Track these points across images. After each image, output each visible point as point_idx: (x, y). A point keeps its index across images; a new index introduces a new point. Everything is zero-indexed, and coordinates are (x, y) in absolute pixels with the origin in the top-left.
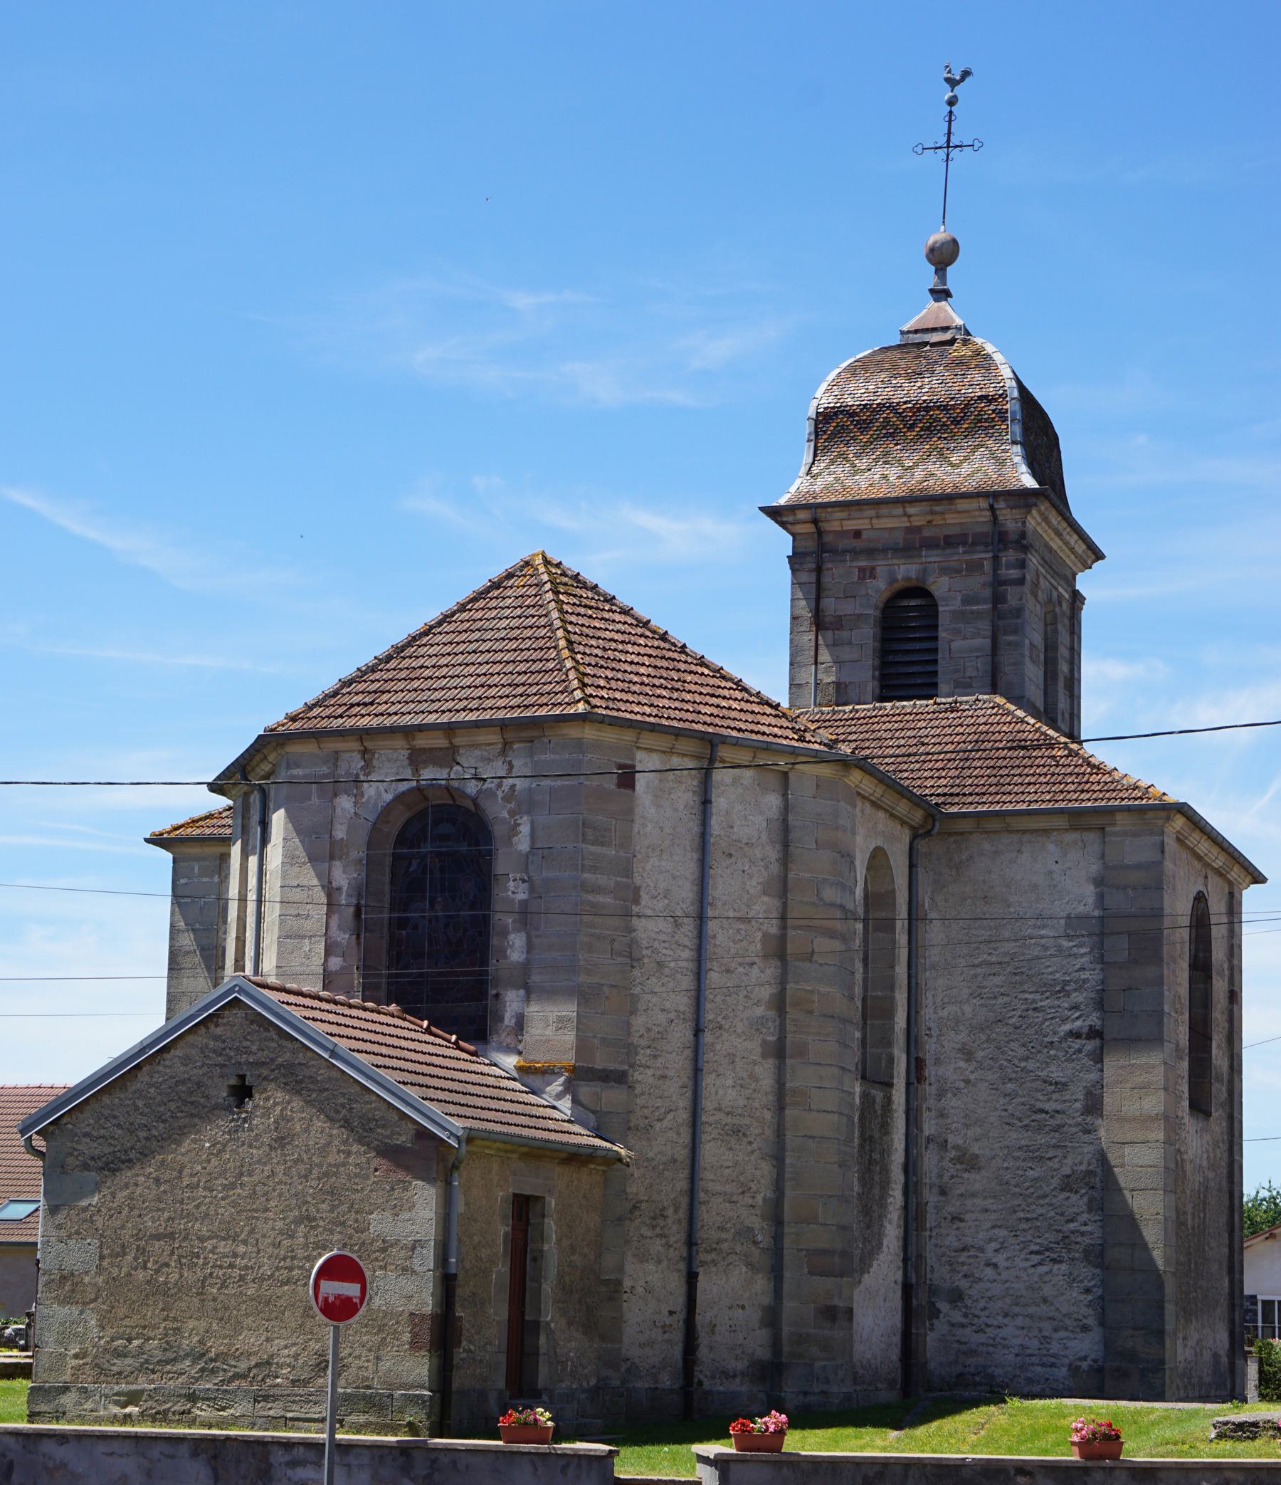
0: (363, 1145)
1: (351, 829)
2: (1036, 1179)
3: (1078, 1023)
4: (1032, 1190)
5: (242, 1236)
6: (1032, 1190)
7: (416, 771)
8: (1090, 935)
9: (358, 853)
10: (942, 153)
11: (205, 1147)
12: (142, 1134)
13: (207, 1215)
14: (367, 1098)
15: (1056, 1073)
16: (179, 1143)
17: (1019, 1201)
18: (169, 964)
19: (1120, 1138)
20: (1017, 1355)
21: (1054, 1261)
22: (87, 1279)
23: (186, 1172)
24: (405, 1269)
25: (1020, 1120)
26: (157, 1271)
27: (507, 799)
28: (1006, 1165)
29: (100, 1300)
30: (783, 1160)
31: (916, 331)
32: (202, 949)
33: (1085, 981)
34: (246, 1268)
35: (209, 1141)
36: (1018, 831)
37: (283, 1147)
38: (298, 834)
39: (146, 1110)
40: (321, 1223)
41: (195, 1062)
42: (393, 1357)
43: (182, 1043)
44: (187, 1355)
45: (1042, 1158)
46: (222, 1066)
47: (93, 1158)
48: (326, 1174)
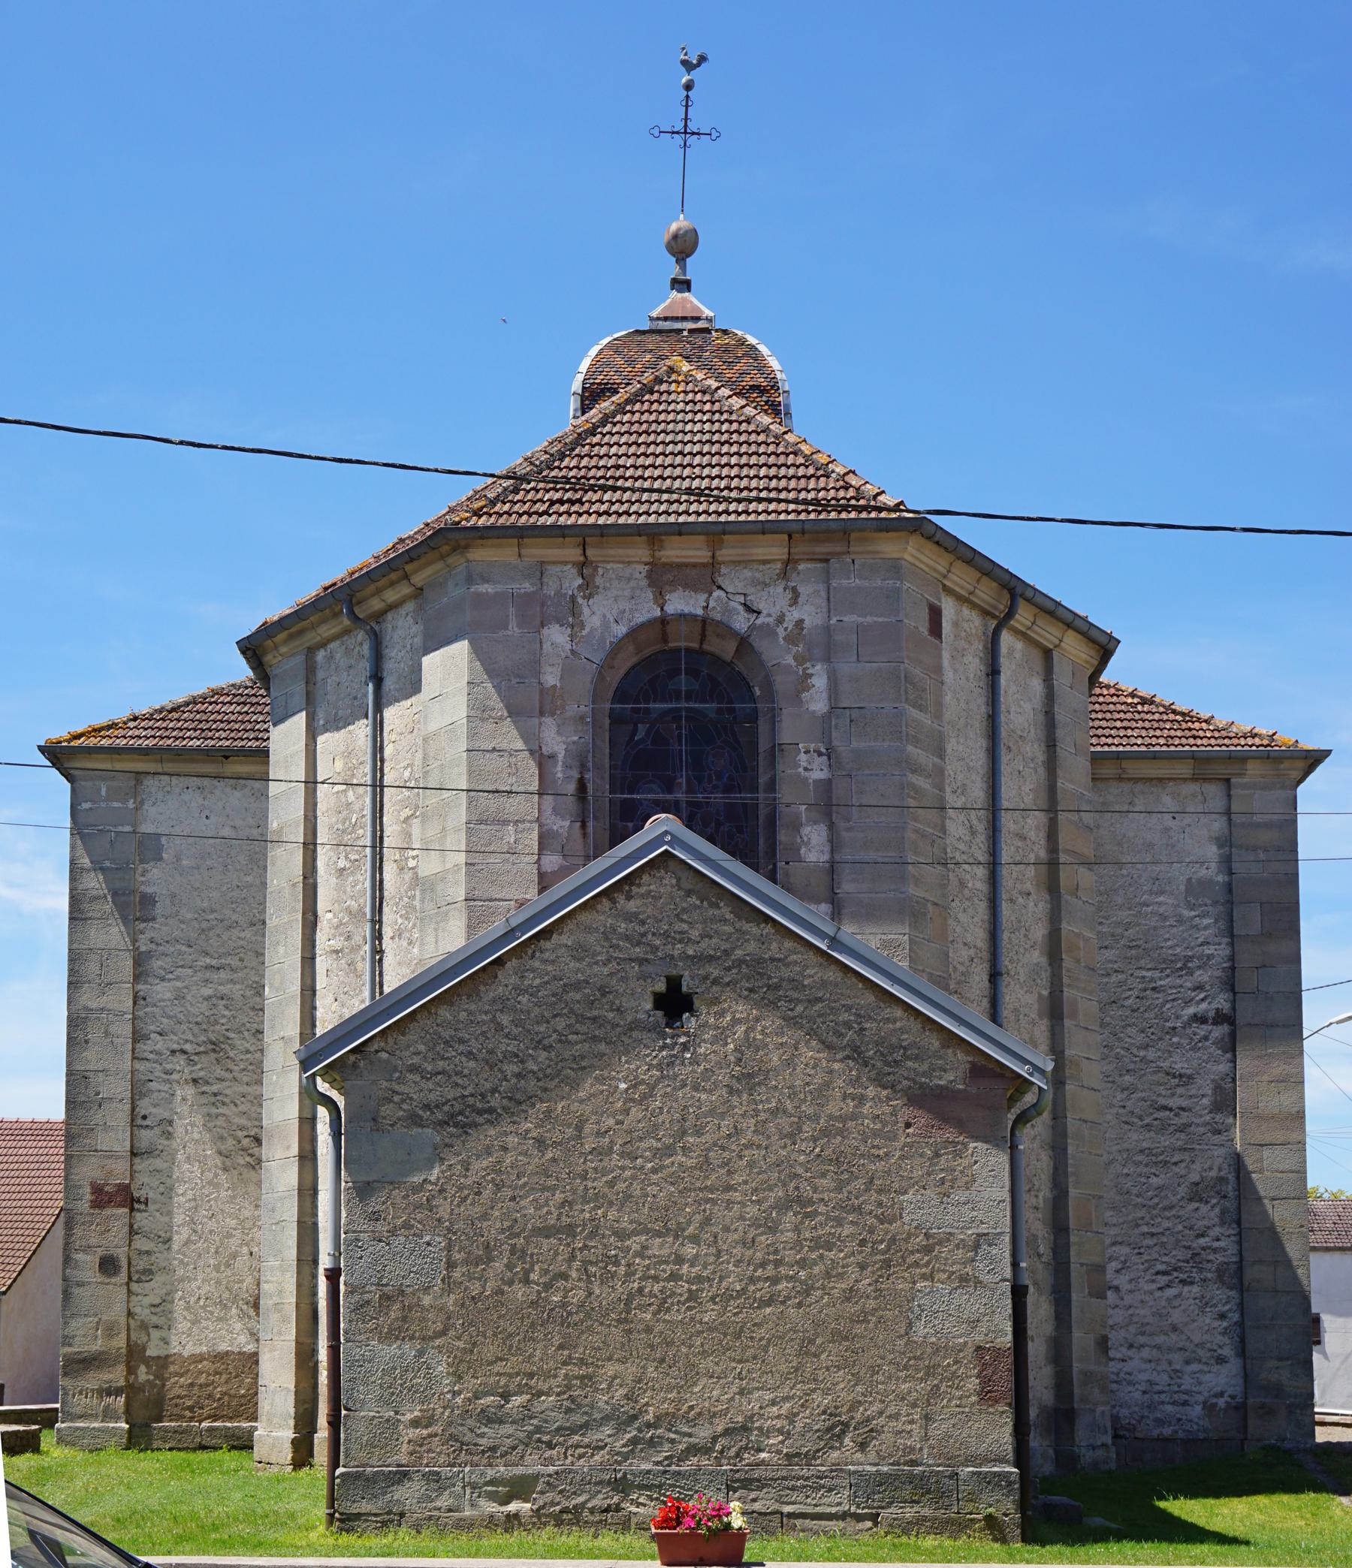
0: (885, 1088)
1: (566, 673)
2: (1160, 1188)
3: (1204, 1006)
4: (1156, 1200)
5: (691, 1230)
6: (1156, 1200)
7: (660, 600)
8: (1215, 903)
9: (579, 706)
10: (679, 139)
11: (624, 1092)
12: (511, 1068)
13: (628, 1197)
14: (887, 1012)
15: (1179, 1064)
16: (575, 1086)
17: (1142, 1213)
18: (70, 913)
19: (1259, 1139)
20: (1145, 1392)
21: (1183, 1282)
22: (427, 1300)
23: (588, 1128)
24: (964, 1279)
25: (1141, 1118)
26: (548, 1286)
27: (791, 640)
28: (1125, 1171)
29: (452, 1333)
30: (1065, 1150)
31: (666, 319)
32: (115, 894)
33: (1210, 957)
34: (699, 1279)
35: (625, 1080)
36: (1129, 779)
37: (751, 1090)
38: (490, 677)
39: (515, 1031)
40: (822, 1209)
41: (595, 954)
42: (953, 1415)
43: (571, 925)
44: (607, 1418)
45: (1166, 1163)
46: (642, 961)
47: (427, 1107)
48: (825, 1133)
